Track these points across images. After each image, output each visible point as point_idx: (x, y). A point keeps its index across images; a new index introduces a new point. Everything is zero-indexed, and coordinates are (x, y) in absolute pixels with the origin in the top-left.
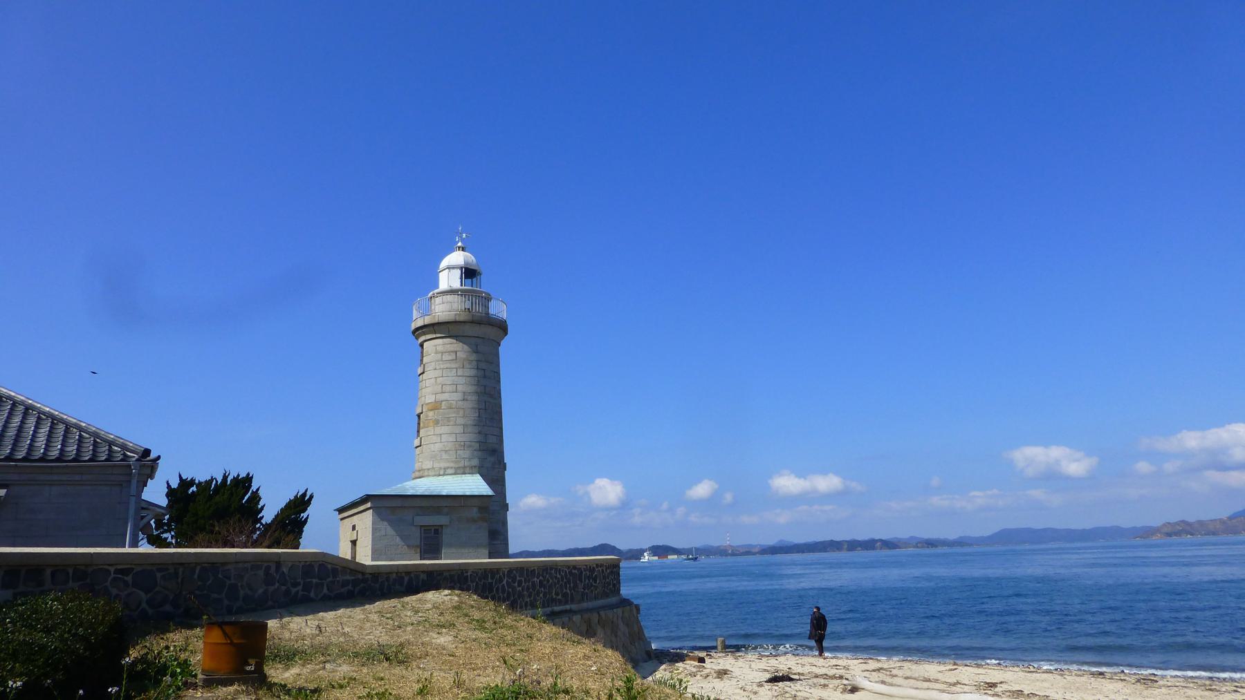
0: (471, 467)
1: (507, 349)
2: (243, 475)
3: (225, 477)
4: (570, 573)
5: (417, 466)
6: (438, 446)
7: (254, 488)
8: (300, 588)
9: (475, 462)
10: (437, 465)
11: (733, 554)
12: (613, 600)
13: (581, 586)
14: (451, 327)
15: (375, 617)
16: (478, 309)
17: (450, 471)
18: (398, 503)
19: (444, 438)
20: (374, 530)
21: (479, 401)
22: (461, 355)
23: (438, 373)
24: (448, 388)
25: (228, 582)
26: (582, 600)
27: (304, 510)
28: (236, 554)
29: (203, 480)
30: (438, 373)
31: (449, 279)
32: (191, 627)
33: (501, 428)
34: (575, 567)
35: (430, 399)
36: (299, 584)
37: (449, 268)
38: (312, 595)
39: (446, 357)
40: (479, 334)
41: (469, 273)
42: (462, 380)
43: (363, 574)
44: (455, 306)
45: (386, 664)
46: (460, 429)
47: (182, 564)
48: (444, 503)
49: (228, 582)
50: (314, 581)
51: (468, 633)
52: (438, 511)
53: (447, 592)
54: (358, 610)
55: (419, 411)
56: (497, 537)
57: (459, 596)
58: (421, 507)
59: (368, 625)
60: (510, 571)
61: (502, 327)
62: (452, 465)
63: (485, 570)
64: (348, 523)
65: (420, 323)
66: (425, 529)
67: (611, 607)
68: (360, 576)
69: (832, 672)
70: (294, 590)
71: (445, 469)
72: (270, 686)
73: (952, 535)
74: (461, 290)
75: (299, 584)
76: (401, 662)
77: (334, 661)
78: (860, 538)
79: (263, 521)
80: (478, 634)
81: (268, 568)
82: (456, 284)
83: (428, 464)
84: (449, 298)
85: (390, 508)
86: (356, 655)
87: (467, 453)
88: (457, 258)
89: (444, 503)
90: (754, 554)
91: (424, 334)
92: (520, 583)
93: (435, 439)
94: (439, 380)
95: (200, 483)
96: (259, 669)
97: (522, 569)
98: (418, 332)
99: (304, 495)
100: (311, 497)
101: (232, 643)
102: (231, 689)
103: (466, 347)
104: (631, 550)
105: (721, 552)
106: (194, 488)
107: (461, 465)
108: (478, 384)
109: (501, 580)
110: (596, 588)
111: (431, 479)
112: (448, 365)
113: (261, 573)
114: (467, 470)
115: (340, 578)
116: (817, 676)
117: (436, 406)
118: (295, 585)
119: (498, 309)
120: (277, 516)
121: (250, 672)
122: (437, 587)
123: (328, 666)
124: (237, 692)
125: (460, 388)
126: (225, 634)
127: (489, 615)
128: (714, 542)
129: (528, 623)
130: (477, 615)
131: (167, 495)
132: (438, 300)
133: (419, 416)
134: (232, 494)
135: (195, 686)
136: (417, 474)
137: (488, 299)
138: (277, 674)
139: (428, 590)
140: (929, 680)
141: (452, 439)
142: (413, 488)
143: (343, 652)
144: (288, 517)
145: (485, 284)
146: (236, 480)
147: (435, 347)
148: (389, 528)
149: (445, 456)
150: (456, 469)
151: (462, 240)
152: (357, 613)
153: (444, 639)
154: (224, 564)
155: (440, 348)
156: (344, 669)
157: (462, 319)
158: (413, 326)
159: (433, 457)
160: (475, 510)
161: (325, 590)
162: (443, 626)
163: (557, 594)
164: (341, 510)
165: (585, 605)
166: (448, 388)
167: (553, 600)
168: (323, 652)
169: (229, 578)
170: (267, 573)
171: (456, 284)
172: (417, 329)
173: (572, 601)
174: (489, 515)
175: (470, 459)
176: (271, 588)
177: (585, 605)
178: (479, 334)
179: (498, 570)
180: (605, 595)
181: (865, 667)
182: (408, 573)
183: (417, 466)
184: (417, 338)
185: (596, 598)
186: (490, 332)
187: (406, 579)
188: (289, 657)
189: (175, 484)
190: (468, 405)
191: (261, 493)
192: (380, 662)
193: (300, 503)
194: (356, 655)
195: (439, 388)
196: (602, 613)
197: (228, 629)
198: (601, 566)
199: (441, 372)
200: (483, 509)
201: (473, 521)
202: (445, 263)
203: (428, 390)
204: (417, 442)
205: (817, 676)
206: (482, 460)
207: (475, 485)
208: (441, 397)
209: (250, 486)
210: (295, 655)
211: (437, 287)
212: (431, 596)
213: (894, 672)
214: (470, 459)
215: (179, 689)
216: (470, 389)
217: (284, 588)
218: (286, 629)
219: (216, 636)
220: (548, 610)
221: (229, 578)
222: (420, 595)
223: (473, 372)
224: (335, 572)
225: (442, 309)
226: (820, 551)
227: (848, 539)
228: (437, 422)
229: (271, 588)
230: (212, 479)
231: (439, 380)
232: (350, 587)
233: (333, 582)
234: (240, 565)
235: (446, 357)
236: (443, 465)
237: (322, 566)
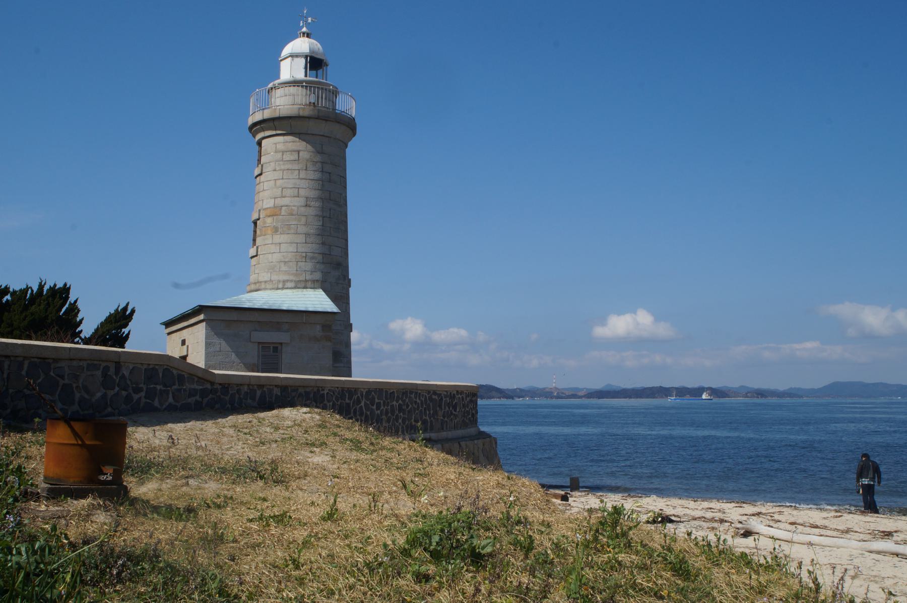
0: (314, 281)
2: (60, 285)
3: (41, 287)
4: (431, 399)
5: (253, 278)
6: (276, 257)
7: (72, 299)
8: (143, 394)
9: (318, 276)
10: (275, 277)
11: (558, 397)
12: (471, 431)
13: (440, 413)
15: (231, 431)
16: (323, 103)
17: (289, 285)
18: (234, 316)
20: (208, 345)
21: (323, 209)
22: (305, 155)
23: (278, 175)
24: (288, 192)
25: (61, 382)
26: (442, 429)
27: (126, 326)
28: (70, 349)
29: (17, 289)
30: (278, 175)
31: (291, 69)
32: (22, 431)
33: (347, 240)
34: (435, 393)
35: (268, 203)
36: (140, 390)
37: (293, 56)
38: (156, 403)
39: (288, 157)
40: (324, 131)
41: (315, 63)
42: (304, 184)
43: (212, 383)
44: (299, 100)
45: (261, 483)
46: (301, 239)
47: (7, 357)
49: (61, 382)
50: (159, 387)
51: (342, 452)
53: (305, 410)
54: (210, 423)
55: (255, 216)
56: (341, 359)
57: (319, 414)
59: (225, 439)
60: (369, 392)
61: (350, 126)
62: (292, 278)
63: (343, 389)
64: (177, 337)
65: (258, 117)
66: (264, 346)
67: (472, 438)
68: (208, 386)
69: (709, 515)
70: (136, 397)
71: (284, 282)
72: (134, 501)
73: (781, 387)
74: (307, 82)
75: (140, 390)
76: (277, 482)
77: (198, 476)
78: (690, 386)
79: (82, 335)
80: (354, 455)
81: (106, 369)
82: (300, 75)
83: (265, 276)
84: (293, 90)
85: (223, 320)
86: (224, 471)
87: (309, 266)
88: (301, 45)
90: (580, 397)
91: (263, 130)
92: (378, 408)
93: (273, 248)
94: (279, 183)
95: (15, 292)
96: (117, 480)
97: (381, 390)
98: (255, 127)
99: (125, 309)
100: (133, 311)
101: (83, 445)
102: (84, 502)
103: (309, 147)
105: (546, 394)
106: (8, 297)
107: (302, 278)
108: (322, 189)
109: (359, 402)
110: (456, 416)
111: (268, 292)
112: (287, 167)
113: (99, 373)
114: (309, 284)
115: (187, 386)
116: (695, 519)
117: (275, 212)
118: (137, 390)
119: (347, 105)
120: (97, 330)
121: (105, 483)
122: (292, 405)
123: (191, 481)
124: (93, 507)
126: (76, 434)
127: (362, 436)
128: (540, 384)
129: (409, 446)
130: (348, 435)
132: (279, 92)
133: (255, 223)
134: (48, 304)
135: (37, 497)
136: (253, 287)
137: (335, 93)
138: (144, 489)
139: (283, 406)
140: (817, 527)
141: (292, 248)
142: (249, 301)
143: (207, 467)
144: (109, 331)
145: (332, 76)
146: (53, 290)
147: (276, 145)
148: (224, 343)
149: (284, 268)
151: (308, 25)
152: (210, 427)
153: (320, 458)
154: (56, 360)
155: (280, 147)
156: (211, 488)
157: (307, 112)
158: (251, 121)
159: (272, 269)
160: (318, 327)
161: (171, 400)
162: (313, 445)
163: (417, 421)
164: (168, 324)
165: (444, 434)
166: (288, 192)
168: (180, 465)
169: (62, 377)
170: (105, 375)
171: (300, 75)
172: (255, 124)
173: (432, 429)
174: (330, 333)
175: (312, 272)
176: (110, 393)
177: (444, 434)
178: (324, 131)
179: (356, 390)
180: (465, 425)
181: (741, 511)
182: (261, 386)
183: (253, 278)
184: (254, 137)
185: (455, 428)
187: (259, 393)
188: (145, 469)
190: (311, 211)
191: (80, 305)
192: (253, 480)
193: (120, 319)
194: (224, 471)
195: (278, 192)
196: (463, 444)
197: (77, 426)
198: (462, 393)
199: (280, 175)
200: (326, 327)
202: (287, 50)
203: (266, 194)
204: (252, 252)
205: (695, 519)
206: (325, 274)
207: (317, 300)
208: (280, 202)
209: (67, 298)
210: (150, 467)
211: (278, 78)
212: (288, 413)
213: (776, 517)
214: (312, 272)
215: (16, 500)
216: (313, 194)
217: (124, 393)
218: (142, 438)
219: (61, 434)
220: (427, 435)
221: (62, 377)
222: (275, 412)
223: (317, 175)
224: (181, 379)
225: (284, 102)
226: (648, 397)
227: (677, 386)
228: (276, 230)
229: (110, 393)
230: (27, 288)
231: (279, 183)
232: (198, 398)
233: (179, 390)
234: (75, 363)
235: (288, 157)
236: (286, 278)
237: (167, 371)
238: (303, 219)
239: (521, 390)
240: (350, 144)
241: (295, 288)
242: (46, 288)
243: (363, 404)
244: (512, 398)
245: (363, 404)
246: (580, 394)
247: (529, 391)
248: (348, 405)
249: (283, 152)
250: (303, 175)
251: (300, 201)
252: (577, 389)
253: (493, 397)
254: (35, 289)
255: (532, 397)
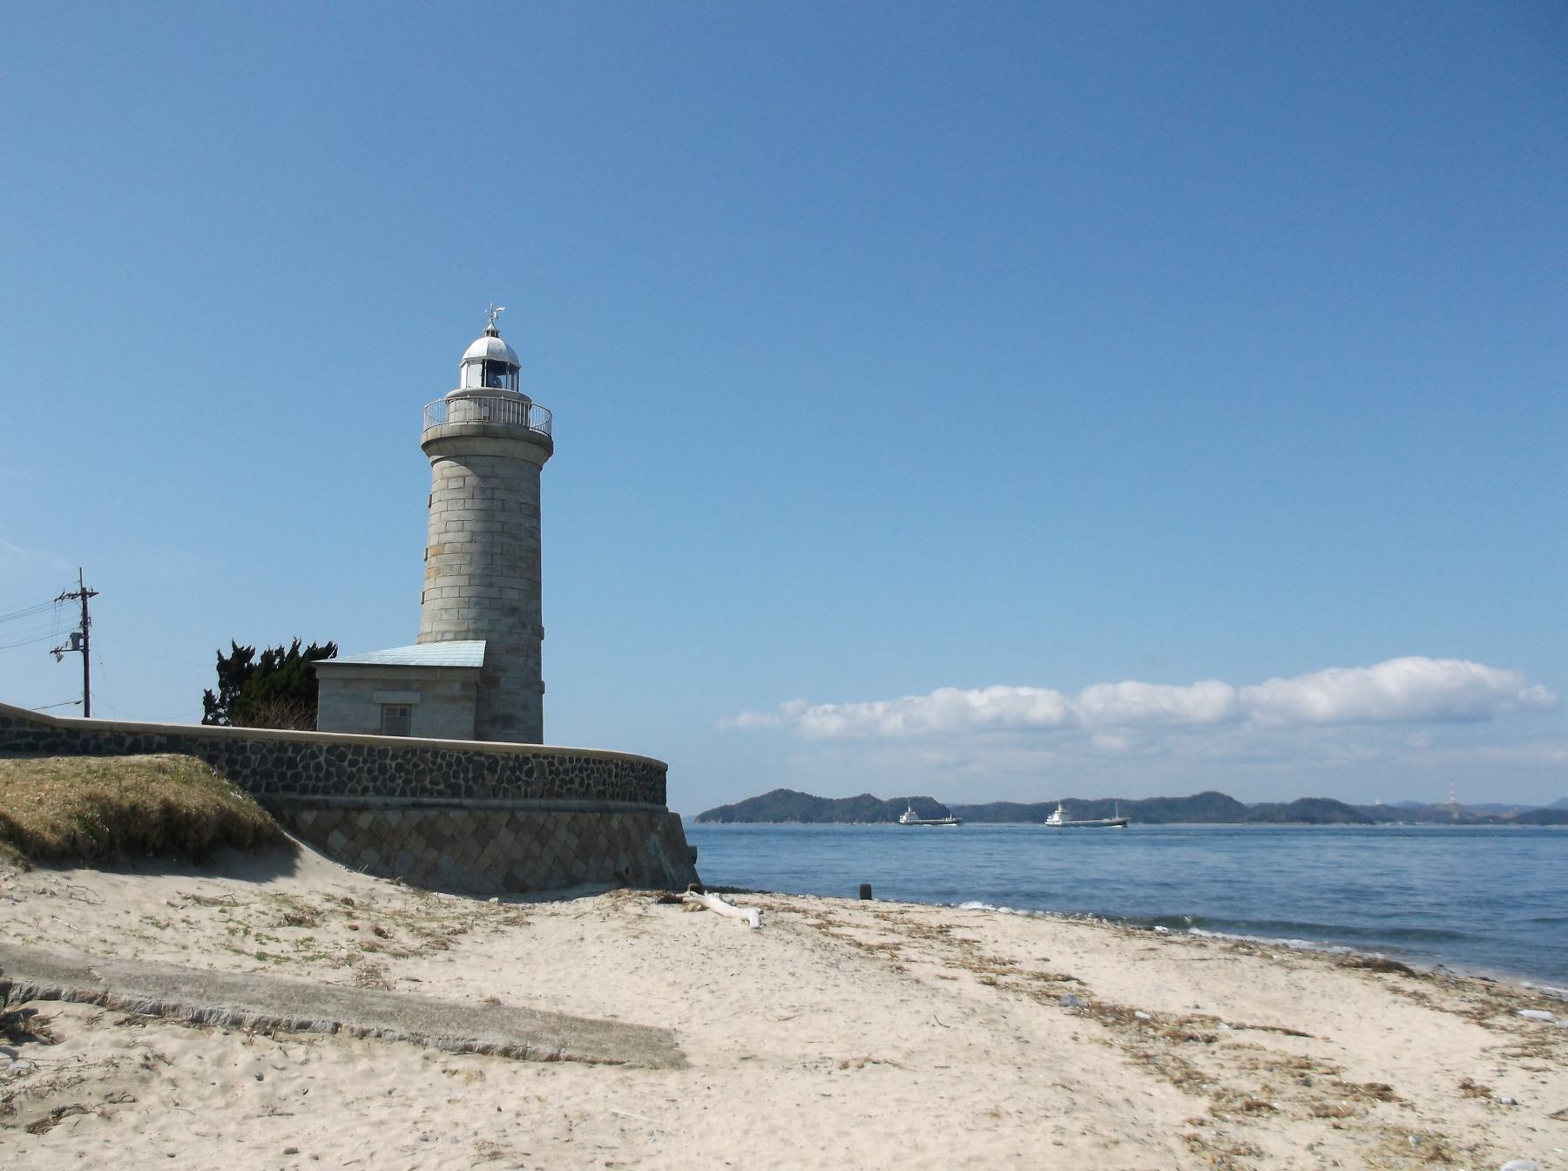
1: (551, 475)
3: (295, 648)
11: (1462, 821)
14: (457, 443)
16: (504, 417)
17: (448, 636)
18: (354, 674)
19: (446, 592)
24: (452, 526)
41: (494, 368)
43: (53, 728)
46: (464, 581)
48: (413, 676)
52: (405, 686)
58: (384, 681)
68: (48, 730)
88: (480, 347)
89: (413, 676)
90: (1507, 821)
104: (1262, 806)
107: (464, 627)
112: (454, 495)
114: (471, 635)
125: (467, 525)
131: (219, 668)
150: (456, 633)
155: (447, 473)
157: (469, 431)
158: (423, 440)
160: (457, 685)
167: (424, 790)
185: (533, 796)
186: (517, 449)
189: (228, 655)
201: (453, 699)
216: (477, 527)
235: (453, 484)
236: (446, 628)
238: (468, 557)
239: (1389, 809)
240: (545, 466)
241: (455, 639)
242: (302, 652)
243: (322, 759)
244: (1371, 822)
245: (322, 759)
246: (1504, 816)
247: (1404, 810)
248: (293, 759)
249: (449, 479)
250: (469, 504)
251: (462, 537)
252: (1500, 807)
253: (1334, 821)
254: (287, 652)
255: (1410, 822)
